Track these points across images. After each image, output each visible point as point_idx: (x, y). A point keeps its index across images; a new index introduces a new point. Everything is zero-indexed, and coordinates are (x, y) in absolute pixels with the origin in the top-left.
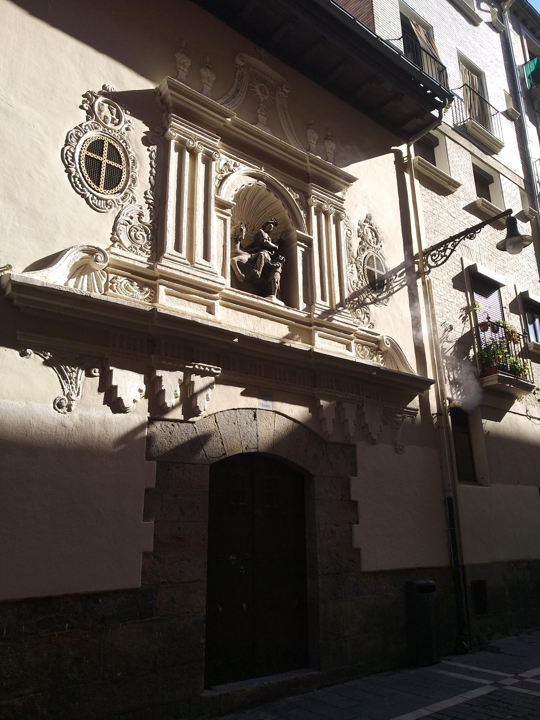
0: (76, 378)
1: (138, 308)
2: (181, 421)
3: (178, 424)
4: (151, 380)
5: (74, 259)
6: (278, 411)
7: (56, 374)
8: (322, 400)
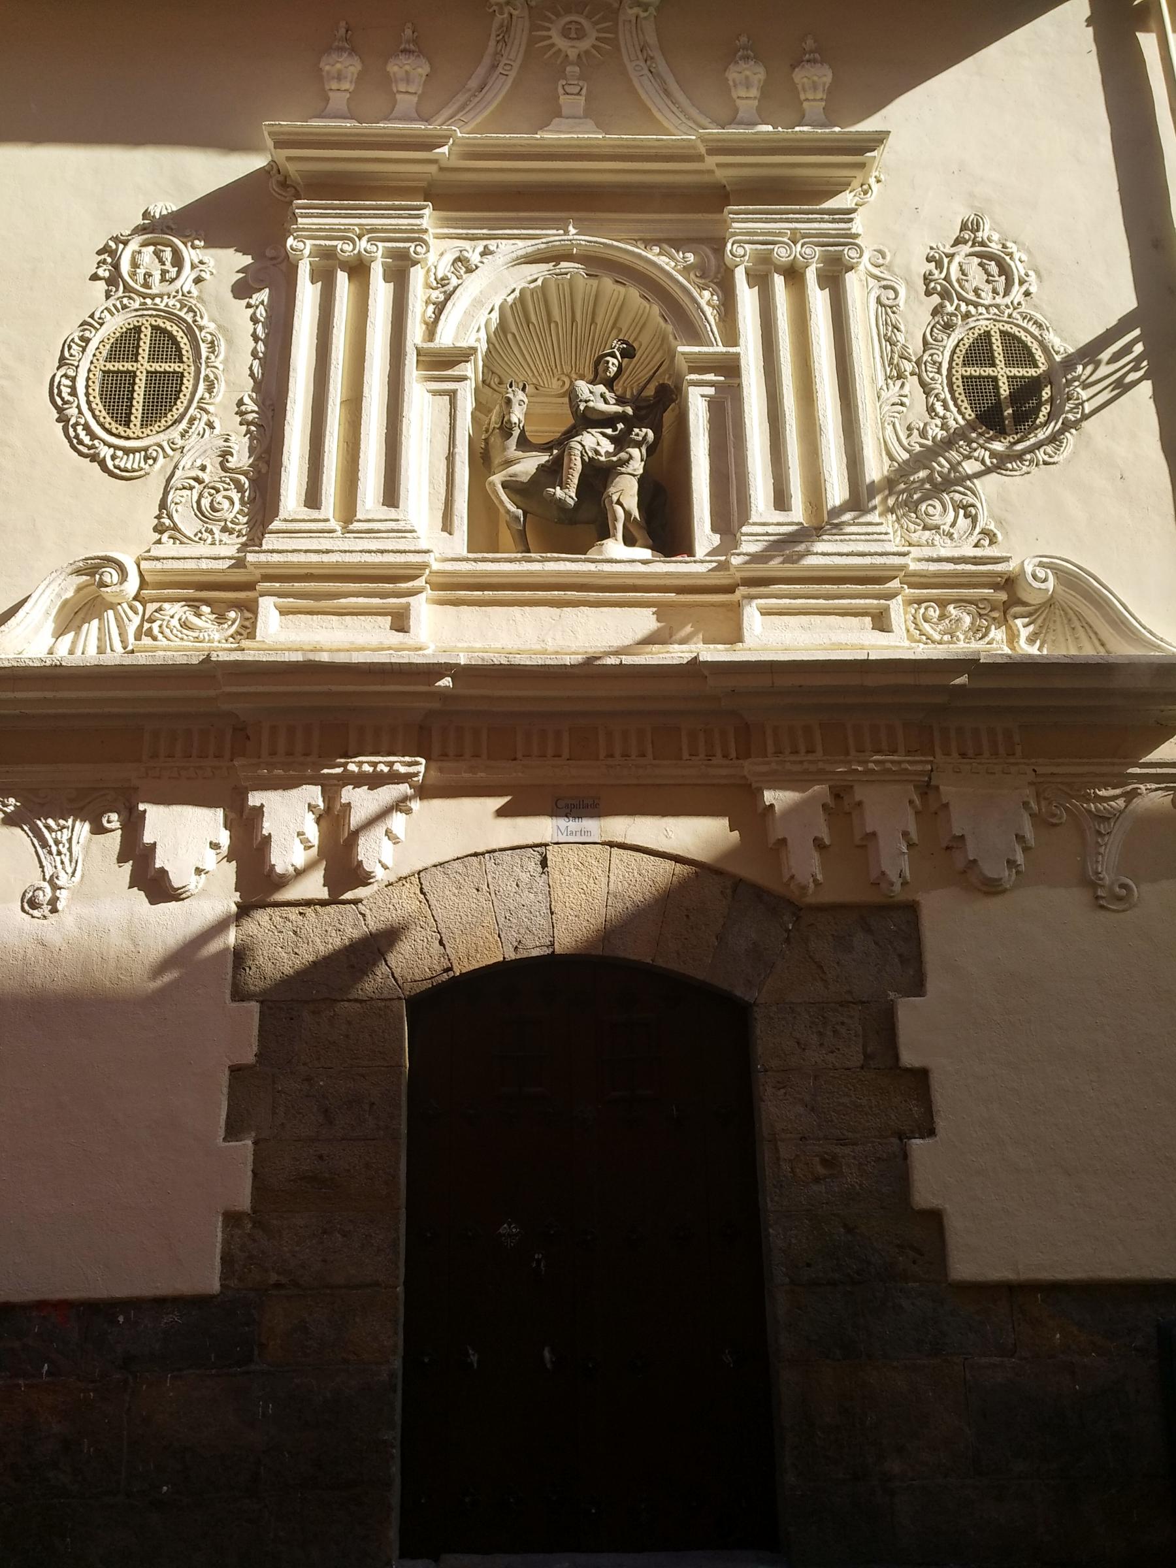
0: (70, 840)
1: (171, 663)
2: (323, 903)
3: (316, 912)
4: (244, 817)
5: (59, 595)
6: (620, 840)
7: (28, 839)
8: (769, 788)
